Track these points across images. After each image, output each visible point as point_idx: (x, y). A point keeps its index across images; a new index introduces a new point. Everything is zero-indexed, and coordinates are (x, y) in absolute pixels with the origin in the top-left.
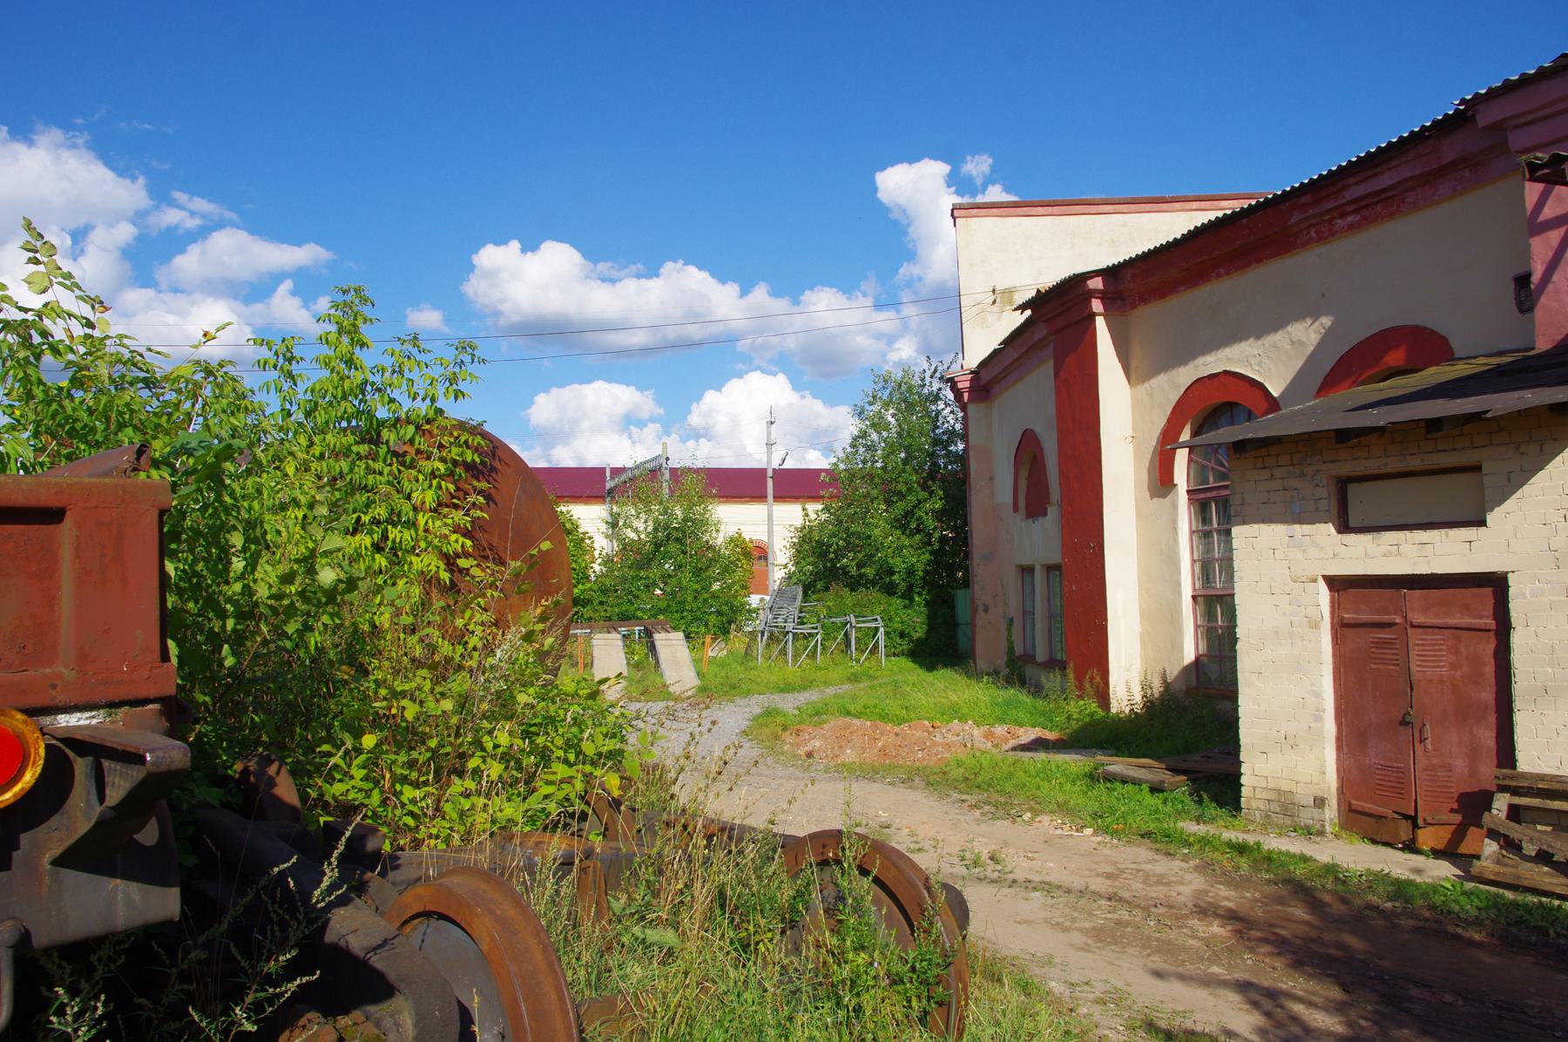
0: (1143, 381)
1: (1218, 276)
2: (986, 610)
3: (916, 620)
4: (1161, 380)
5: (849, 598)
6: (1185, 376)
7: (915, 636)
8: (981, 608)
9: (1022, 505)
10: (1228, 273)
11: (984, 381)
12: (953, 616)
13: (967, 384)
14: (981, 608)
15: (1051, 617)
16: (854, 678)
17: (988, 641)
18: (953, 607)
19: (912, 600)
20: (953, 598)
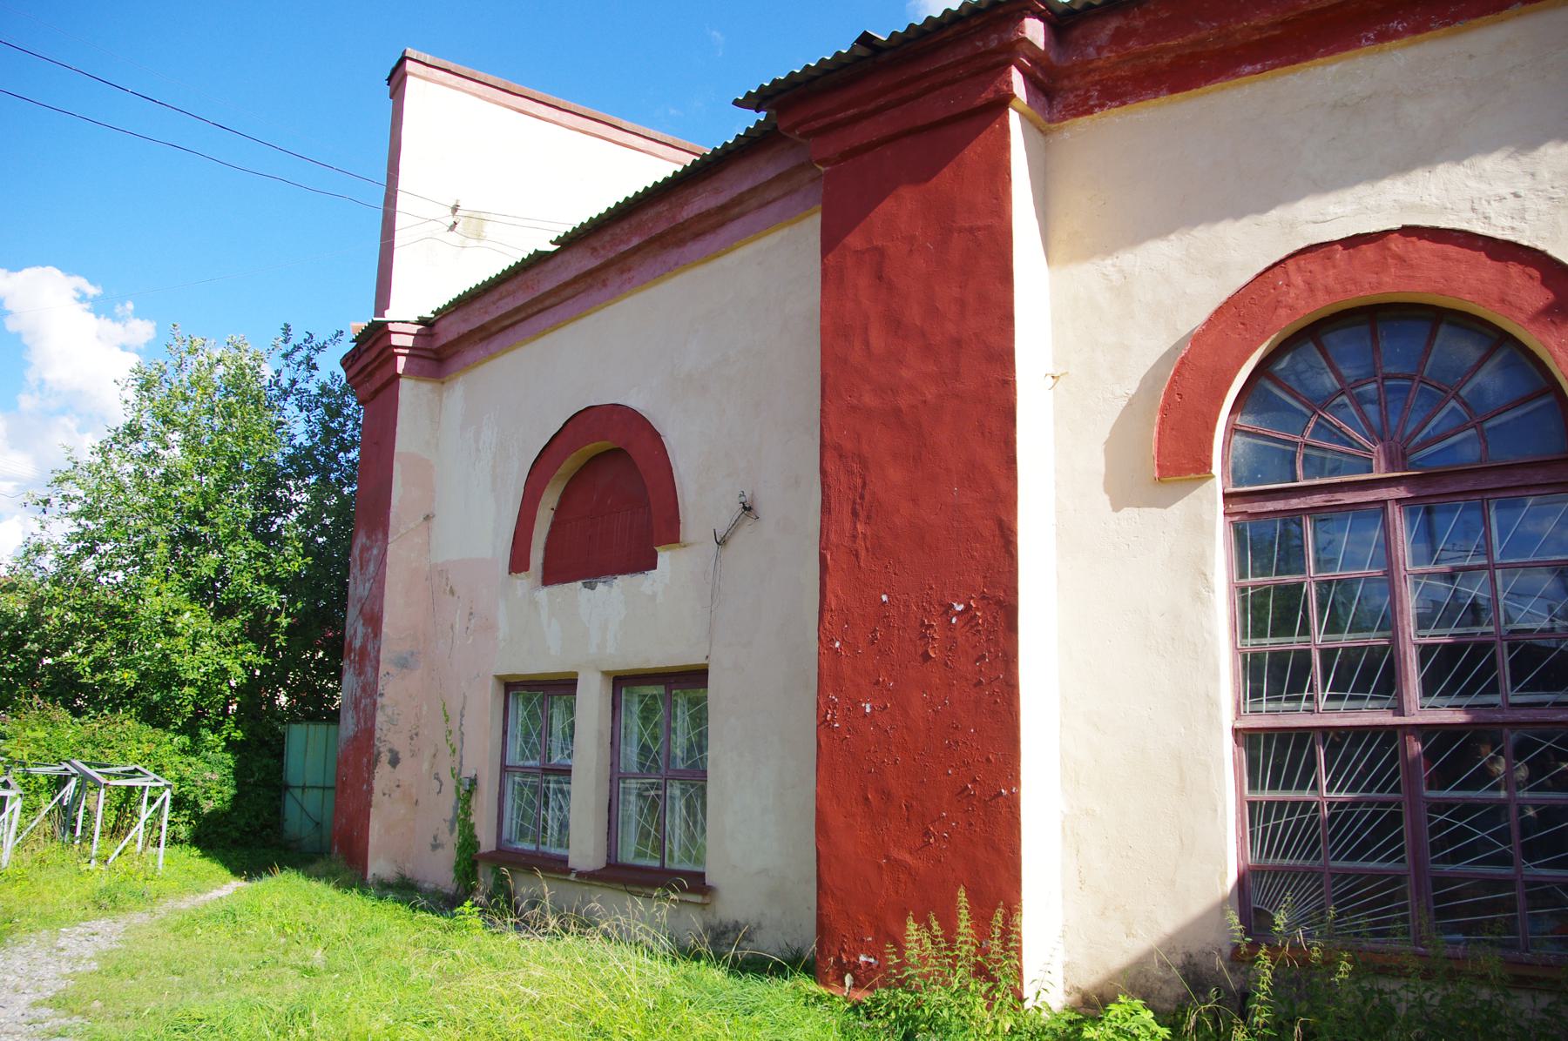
0: (1108, 251)
1: (1383, 37)
2: (395, 761)
3: (213, 779)
4: (1163, 253)
5: (70, 729)
6: (1246, 246)
7: (207, 807)
8: (385, 758)
9: (537, 556)
10: (1418, 29)
11: (443, 340)
12: (280, 769)
13: (409, 341)
14: (385, 758)
15: (616, 776)
16: (106, 902)
17: (406, 819)
18: (279, 755)
19: (195, 737)
20: (281, 739)
